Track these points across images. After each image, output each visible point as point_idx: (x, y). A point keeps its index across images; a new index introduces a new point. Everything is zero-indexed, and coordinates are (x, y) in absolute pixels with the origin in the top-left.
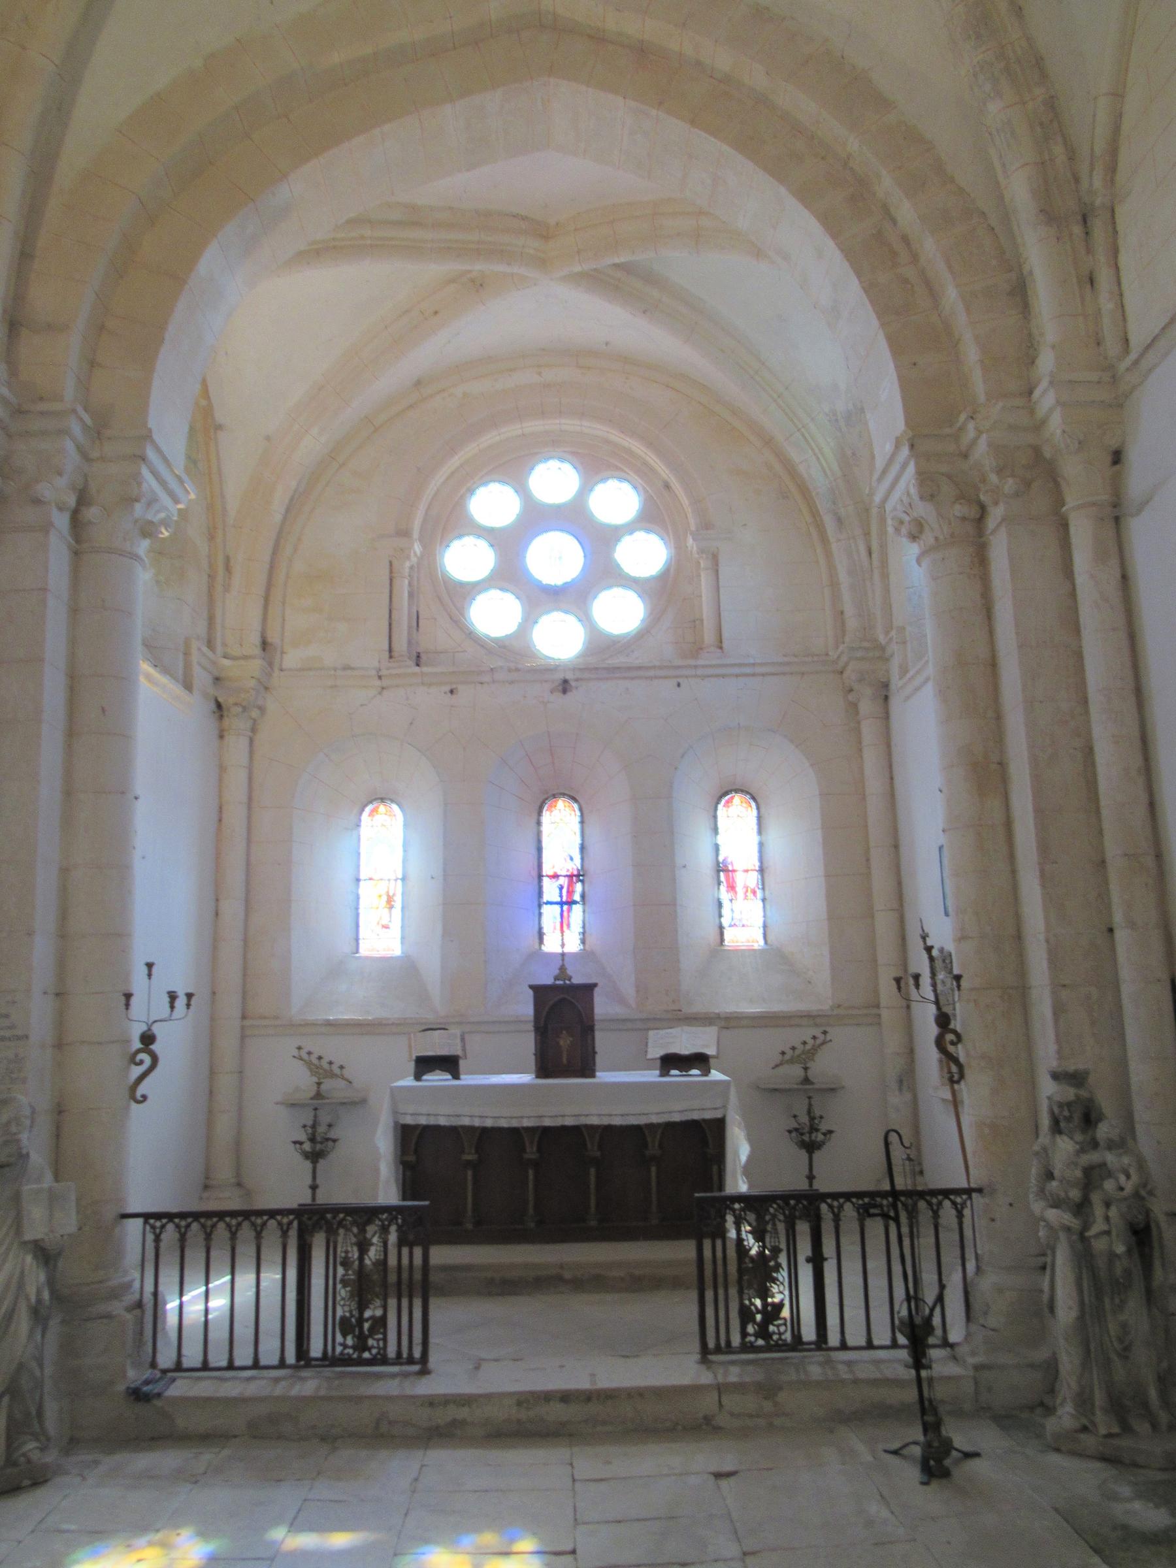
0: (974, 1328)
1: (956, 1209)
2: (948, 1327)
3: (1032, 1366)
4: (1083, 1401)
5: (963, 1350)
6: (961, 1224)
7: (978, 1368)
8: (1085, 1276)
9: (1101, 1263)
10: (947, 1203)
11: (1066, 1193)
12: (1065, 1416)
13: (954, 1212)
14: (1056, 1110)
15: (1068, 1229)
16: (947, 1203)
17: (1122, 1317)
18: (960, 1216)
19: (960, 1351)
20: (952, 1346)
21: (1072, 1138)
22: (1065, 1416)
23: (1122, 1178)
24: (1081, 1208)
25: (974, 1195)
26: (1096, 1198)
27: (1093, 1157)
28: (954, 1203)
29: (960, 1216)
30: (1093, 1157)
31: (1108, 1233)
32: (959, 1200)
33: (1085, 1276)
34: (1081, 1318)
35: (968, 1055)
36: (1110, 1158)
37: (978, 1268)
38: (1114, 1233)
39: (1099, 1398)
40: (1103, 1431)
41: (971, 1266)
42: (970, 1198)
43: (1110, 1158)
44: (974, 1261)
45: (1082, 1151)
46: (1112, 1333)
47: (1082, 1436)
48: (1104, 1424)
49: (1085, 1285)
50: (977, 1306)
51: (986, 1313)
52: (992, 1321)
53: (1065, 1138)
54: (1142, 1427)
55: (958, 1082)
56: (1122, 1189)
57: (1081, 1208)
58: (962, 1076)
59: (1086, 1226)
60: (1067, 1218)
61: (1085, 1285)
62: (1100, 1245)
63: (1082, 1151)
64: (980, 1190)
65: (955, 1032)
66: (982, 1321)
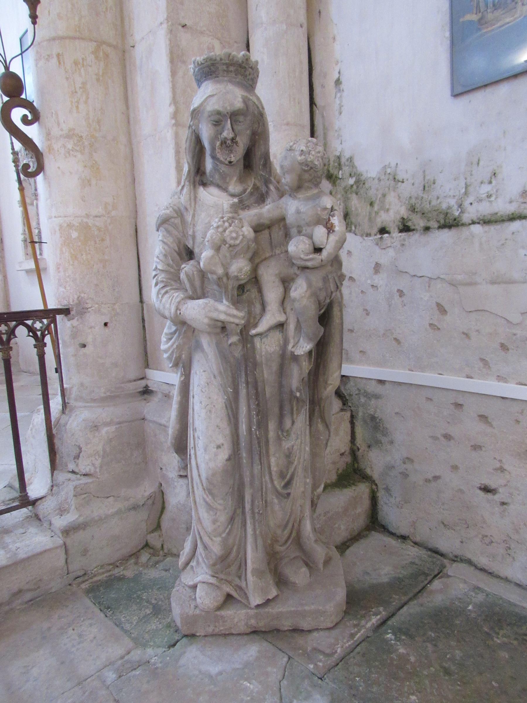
0: (61, 476)
1: (35, 336)
2: (27, 476)
3: (135, 508)
4: (228, 564)
5: (46, 508)
6: (41, 357)
7: (67, 532)
8: (243, 392)
9: (268, 374)
10: (21, 331)
11: (226, 267)
12: (196, 586)
13: (32, 341)
14: (206, 132)
15: (223, 328)
16: (21, 331)
17: (286, 445)
18: (40, 345)
19: (44, 508)
20: (34, 503)
21: (225, 190)
22: (196, 586)
23: (320, 232)
24: (246, 291)
25: (58, 317)
26: (269, 275)
27: (267, 210)
28: (31, 329)
29: (40, 345)
30: (267, 210)
31: (281, 326)
32: (38, 325)
33: (243, 392)
34: (234, 457)
35: (48, 136)
36: (293, 207)
37: (65, 405)
38: (291, 327)
39: (253, 556)
40: (256, 600)
41: (56, 403)
42: (54, 321)
43: (293, 207)
44: (59, 398)
45: (241, 205)
46: (274, 469)
47: (227, 612)
48: (256, 589)
49: (243, 409)
50: (64, 449)
51: (77, 457)
52: (84, 466)
53: (213, 190)
54: (299, 575)
55: (34, 175)
56: (318, 250)
57: (246, 291)
58: (40, 168)
59: (251, 321)
60: (224, 309)
61: (243, 409)
62: (267, 347)
63: (241, 205)
64: (66, 312)
65: (28, 105)
66: (71, 466)
